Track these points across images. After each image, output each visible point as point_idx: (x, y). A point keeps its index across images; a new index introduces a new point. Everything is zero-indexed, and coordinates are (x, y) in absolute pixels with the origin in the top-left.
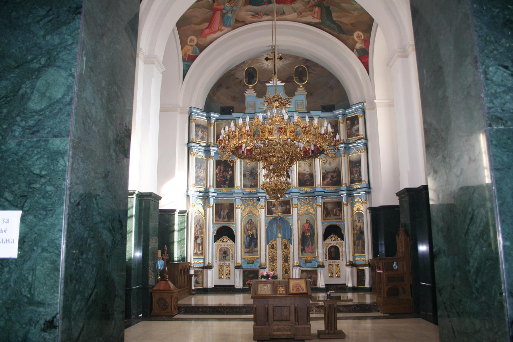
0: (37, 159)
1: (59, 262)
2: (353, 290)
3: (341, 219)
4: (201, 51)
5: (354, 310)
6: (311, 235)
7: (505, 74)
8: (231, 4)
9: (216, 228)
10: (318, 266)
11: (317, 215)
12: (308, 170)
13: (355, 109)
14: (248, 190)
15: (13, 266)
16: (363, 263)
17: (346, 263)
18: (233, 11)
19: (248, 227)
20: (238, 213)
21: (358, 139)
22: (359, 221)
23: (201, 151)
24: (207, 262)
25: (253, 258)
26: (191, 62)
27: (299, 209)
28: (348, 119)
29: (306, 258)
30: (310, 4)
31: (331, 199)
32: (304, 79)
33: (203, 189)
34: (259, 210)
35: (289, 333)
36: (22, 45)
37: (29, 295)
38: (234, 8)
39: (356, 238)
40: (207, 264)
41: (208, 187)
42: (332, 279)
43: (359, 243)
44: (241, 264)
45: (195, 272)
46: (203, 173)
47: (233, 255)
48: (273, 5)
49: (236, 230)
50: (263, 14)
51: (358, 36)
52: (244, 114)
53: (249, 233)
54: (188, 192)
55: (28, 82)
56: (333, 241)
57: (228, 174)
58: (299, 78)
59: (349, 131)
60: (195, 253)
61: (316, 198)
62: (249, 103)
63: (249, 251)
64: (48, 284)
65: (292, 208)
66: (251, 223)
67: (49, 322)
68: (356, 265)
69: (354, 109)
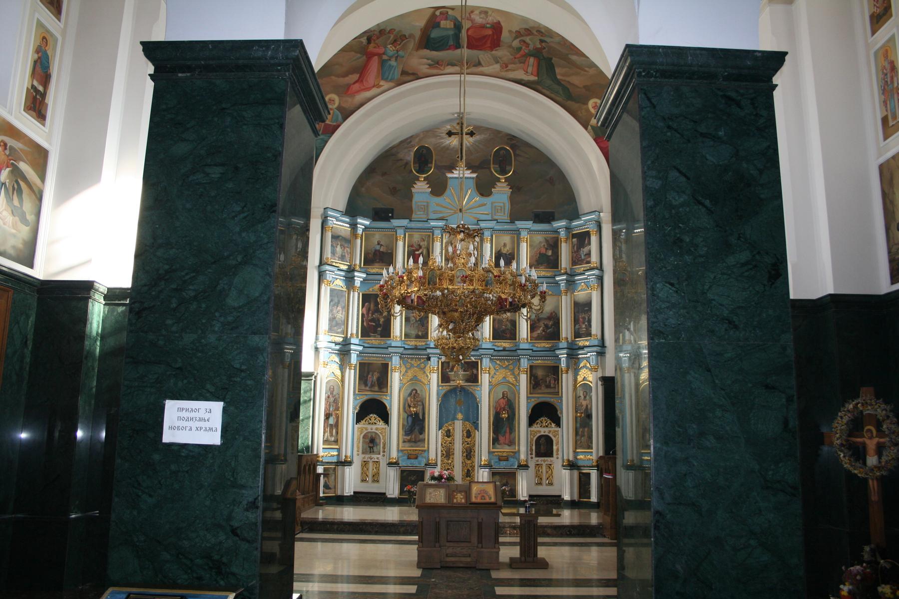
0: (237, 355)
1: (259, 450)
2: (572, 504)
3: (557, 393)
5: (568, 533)
7: (671, 291)
8: (395, 47)
9: (358, 401)
10: (518, 466)
11: (519, 385)
13: (586, 221)
14: (413, 343)
15: (216, 453)
16: (589, 464)
17: (563, 463)
18: (399, 57)
19: (411, 401)
20: (396, 379)
21: (588, 268)
22: (585, 397)
23: (340, 277)
24: (344, 454)
25: (416, 450)
26: (329, 135)
28: (574, 236)
29: (500, 454)
30: (521, 53)
32: (508, 168)
33: (341, 339)
35: (469, 559)
36: (218, 241)
37: (232, 479)
38: (401, 53)
40: (344, 458)
41: (349, 335)
42: (540, 487)
43: (583, 432)
44: (397, 459)
45: (325, 469)
46: (342, 314)
48: (463, 50)
49: (391, 406)
50: (446, 65)
51: (594, 105)
52: (411, 221)
54: (317, 343)
55: (225, 278)
56: (544, 428)
60: (325, 439)
61: (520, 359)
62: (419, 204)
63: (411, 438)
64: (250, 469)
65: (481, 373)
66: (414, 395)
67: (251, 502)
69: (584, 220)
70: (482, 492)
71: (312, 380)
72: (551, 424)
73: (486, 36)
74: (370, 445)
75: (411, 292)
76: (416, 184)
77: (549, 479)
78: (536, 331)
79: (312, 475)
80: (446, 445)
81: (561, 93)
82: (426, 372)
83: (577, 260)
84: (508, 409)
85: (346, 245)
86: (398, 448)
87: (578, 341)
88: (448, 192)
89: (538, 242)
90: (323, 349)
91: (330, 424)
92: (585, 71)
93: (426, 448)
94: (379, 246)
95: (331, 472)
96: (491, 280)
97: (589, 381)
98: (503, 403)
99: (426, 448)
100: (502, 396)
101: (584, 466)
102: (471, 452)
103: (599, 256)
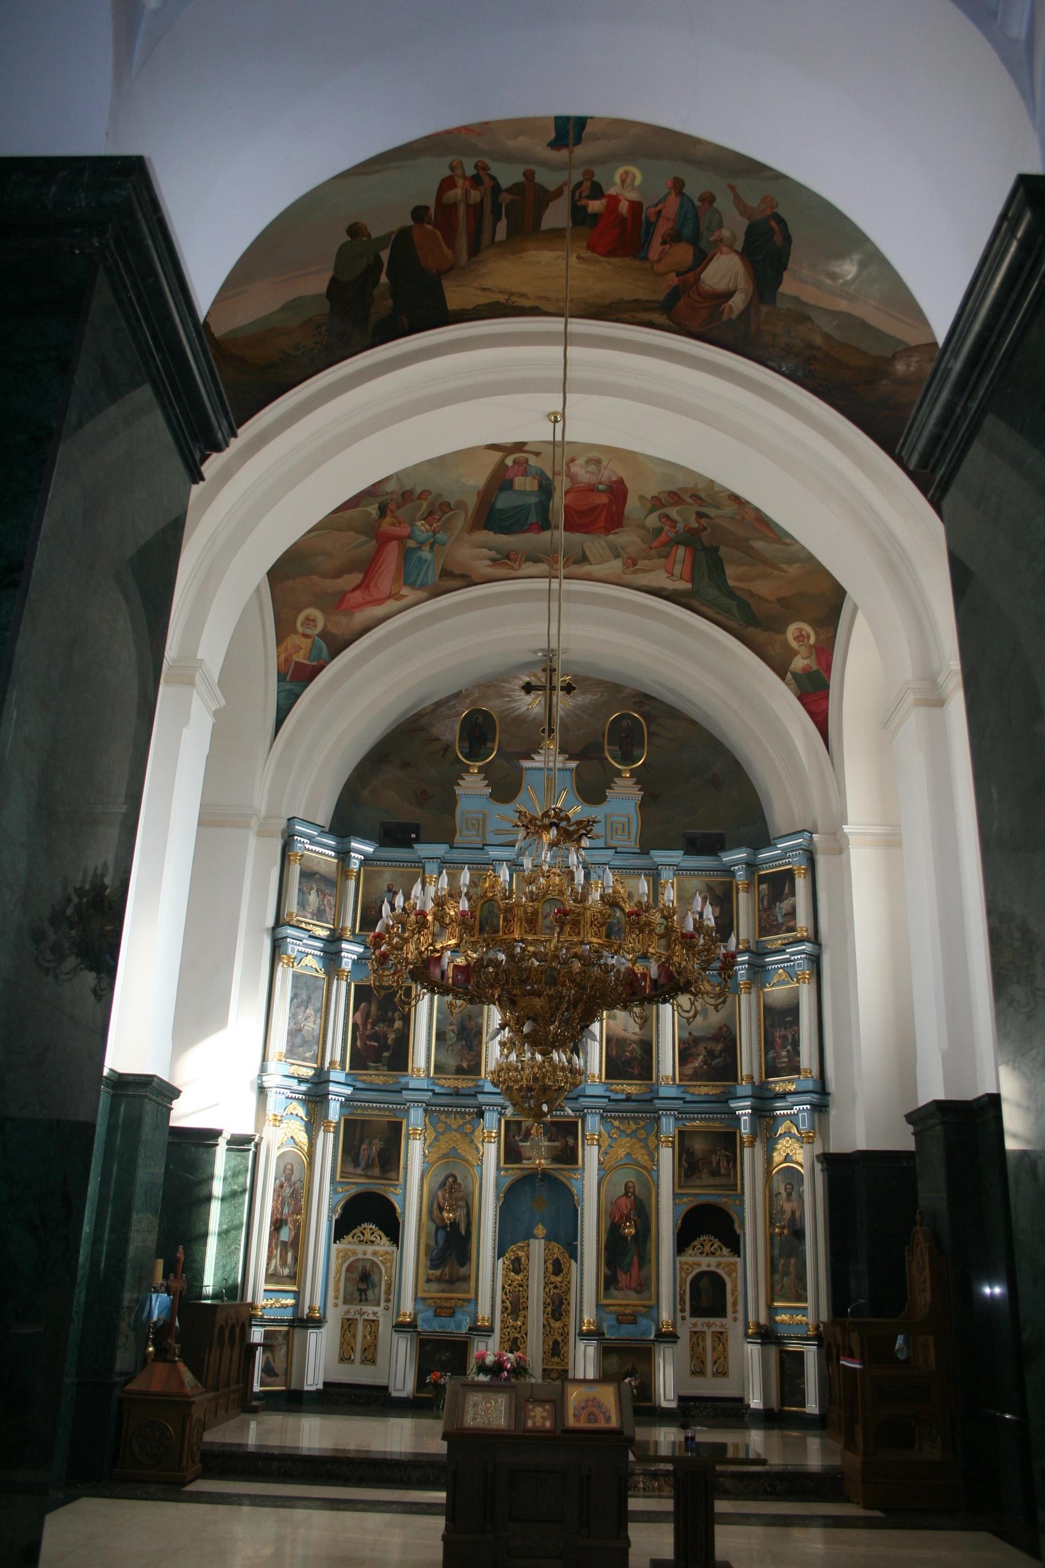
3: (734, 1187)
4: (334, 654)
6: (637, 1232)
8: (431, 525)
9: (340, 1196)
10: (656, 1336)
11: (658, 1170)
14: (450, 1082)
18: (436, 544)
21: (791, 940)
22: (789, 1195)
23: (313, 951)
25: (451, 1299)
27: (602, 1149)
28: (763, 879)
29: (619, 1309)
30: (663, 538)
31: (703, 1124)
32: (636, 752)
33: (311, 1073)
34: (481, 1148)
40: (306, 1311)
41: (327, 1065)
42: (700, 1380)
44: (412, 1316)
45: (267, 1335)
48: (556, 533)
50: (524, 558)
52: (452, 847)
53: (443, 1219)
54: (264, 1078)
58: (620, 748)
60: (270, 1272)
61: (659, 1118)
63: (441, 1274)
66: (451, 1188)
68: (778, 1338)
69: (782, 849)
70: (590, 1403)
71: (249, 1150)
72: (721, 1250)
73: (599, 505)
74: (360, 1286)
75: (442, 948)
77: (719, 1362)
78: (692, 1062)
79: (237, 1348)
81: (736, 612)
83: (768, 926)
84: (636, 1218)
85: (327, 891)
87: (772, 1082)
90: (274, 1090)
92: (782, 570)
93: (472, 1295)
96: (619, 922)
97: (797, 1163)
99: (472, 1295)
100: (623, 1191)
102: (563, 1303)
103: (812, 916)
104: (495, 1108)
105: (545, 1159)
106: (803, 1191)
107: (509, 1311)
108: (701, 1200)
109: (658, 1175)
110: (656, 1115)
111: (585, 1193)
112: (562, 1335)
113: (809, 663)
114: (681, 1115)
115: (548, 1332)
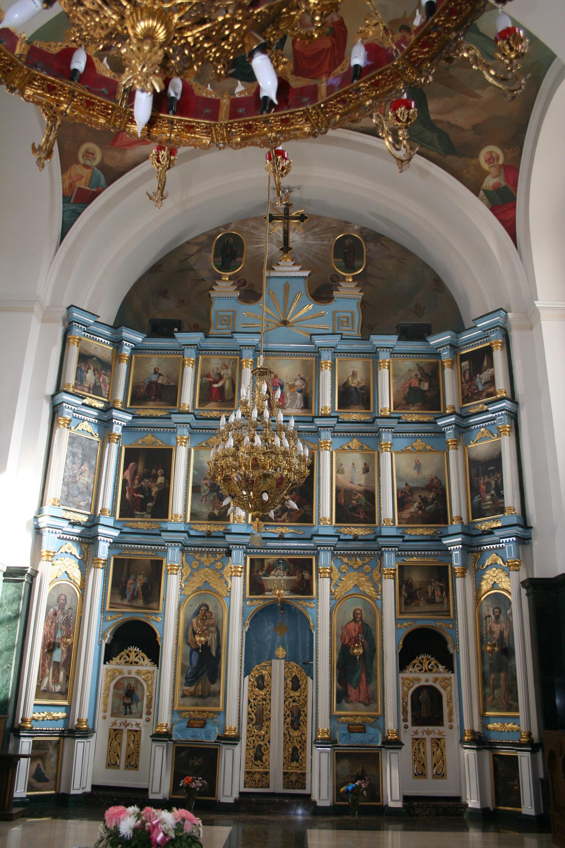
4: (110, 182)
6: (364, 652)
9: (110, 623)
10: (383, 743)
11: (382, 599)
12: (362, 482)
14: (203, 528)
19: (197, 624)
22: (497, 618)
25: (204, 712)
27: (334, 582)
28: (464, 358)
29: (350, 719)
31: (419, 559)
32: (357, 263)
33: (85, 519)
34: (230, 582)
39: (491, 665)
41: (99, 512)
42: (421, 782)
43: (497, 680)
45: (36, 746)
46: (89, 476)
47: (150, 701)
51: (488, 158)
52: (206, 337)
53: (196, 643)
54: (40, 520)
57: (153, 485)
58: (344, 261)
59: (466, 386)
60: (42, 688)
61: (382, 555)
65: (317, 578)
66: (204, 615)
68: (491, 743)
72: (438, 667)
74: (125, 701)
76: (217, 285)
77: (438, 765)
80: (256, 702)
82: (225, 576)
83: (470, 395)
84: (363, 640)
86: (173, 707)
87: (478, 522)
88: (261, 301)
89: (407, 370)
90: (47, 529)
91: (55, 662)
94: (157, 376)
95: (52, 751)
97: (503, 589)
98: (355, 631)
100: (352, 617)
101: (499, 744)
102: (301, 715)
104: (241, 547)
105: (284, 590)
106: (511, 614)
107: (254, 722)
108: (418, 624)
109: (382, 604)
110: (379, 552)
111: (319, 619)
112: (300, 742)
113: (498, 181)
114: (400, 552)
115: (287, 740)
